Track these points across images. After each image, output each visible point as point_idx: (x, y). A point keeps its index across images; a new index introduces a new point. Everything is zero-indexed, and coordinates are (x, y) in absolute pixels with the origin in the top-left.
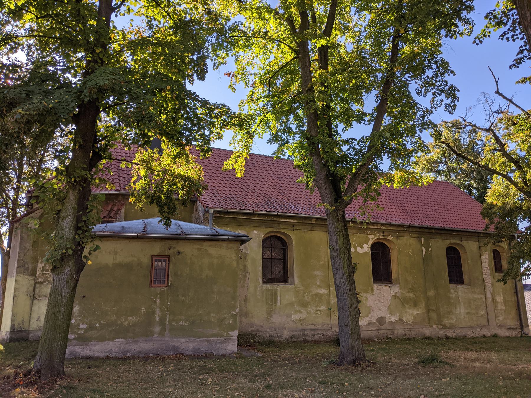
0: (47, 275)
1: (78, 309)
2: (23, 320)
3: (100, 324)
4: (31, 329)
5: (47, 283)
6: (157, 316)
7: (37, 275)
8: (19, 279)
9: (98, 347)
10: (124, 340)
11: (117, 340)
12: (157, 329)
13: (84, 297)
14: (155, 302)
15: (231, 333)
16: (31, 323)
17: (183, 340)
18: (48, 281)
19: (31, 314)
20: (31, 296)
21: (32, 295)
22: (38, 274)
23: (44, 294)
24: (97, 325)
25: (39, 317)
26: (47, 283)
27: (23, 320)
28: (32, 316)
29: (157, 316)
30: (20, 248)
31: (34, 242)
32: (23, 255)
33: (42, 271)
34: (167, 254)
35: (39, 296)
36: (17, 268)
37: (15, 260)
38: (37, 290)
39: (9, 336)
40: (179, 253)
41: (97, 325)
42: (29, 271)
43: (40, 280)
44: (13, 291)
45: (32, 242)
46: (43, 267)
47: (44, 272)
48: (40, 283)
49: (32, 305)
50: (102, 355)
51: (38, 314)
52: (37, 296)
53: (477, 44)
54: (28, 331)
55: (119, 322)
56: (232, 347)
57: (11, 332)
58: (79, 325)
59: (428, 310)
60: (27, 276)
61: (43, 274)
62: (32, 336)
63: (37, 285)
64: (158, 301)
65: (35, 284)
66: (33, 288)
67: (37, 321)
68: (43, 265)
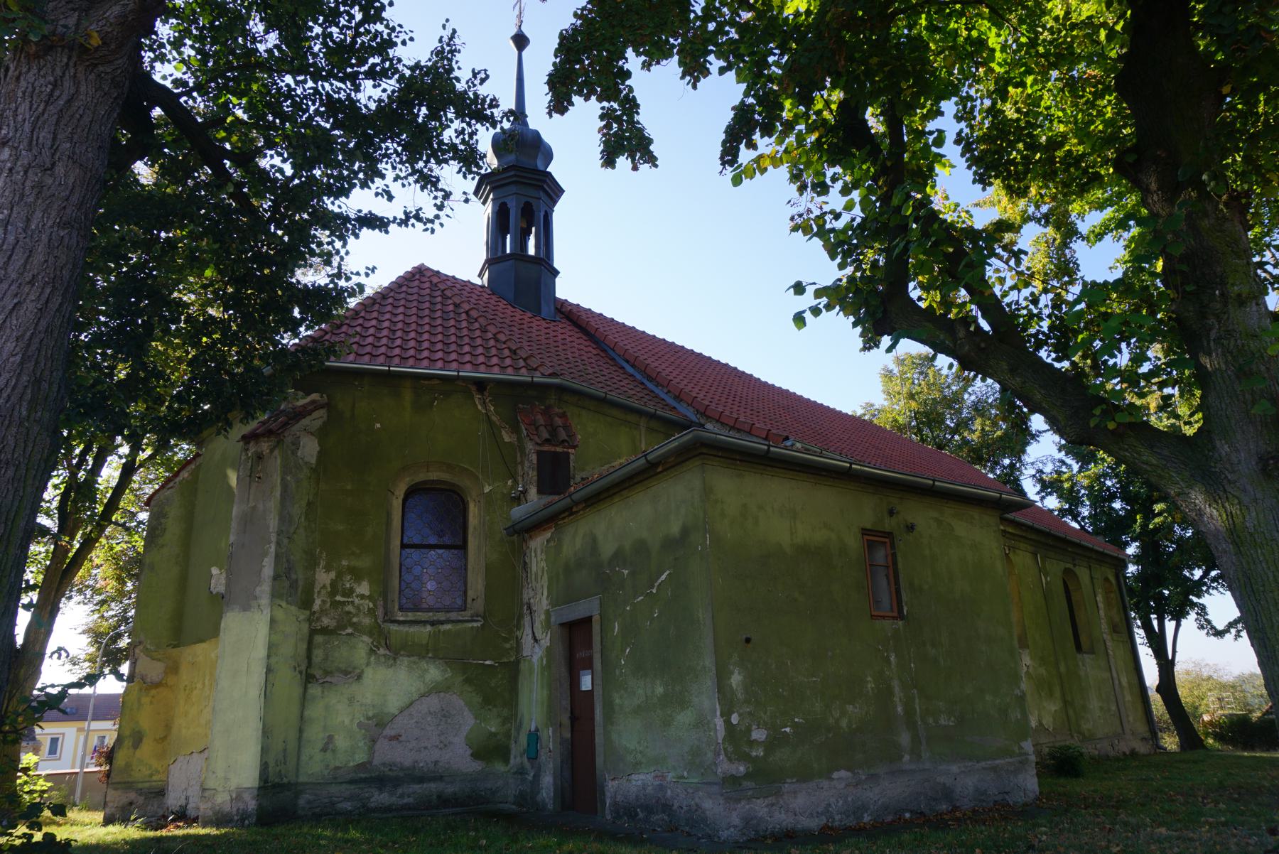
0: (349, 608)
1: (740, 678)
2: (285, 750)
3: (795, 726)
4: (302, 779)
5: (349, 630)
6: (898, 703)
7: (316, 607)
8: (280, 614)
9: (800, 801)
10: (849, 774)
11: (835, 775)
12: (905, 739)
13: (748, 640)
14: (888, 661)
15: (1024, 744)
16: (304, 758)
17: (955, 768)
18: (353, 625)
19: (301, 731)
20: (301, 673)
21: (303, 668)
22: (318, 602)
23: (343, 666)
24: (788, 730)
25: (330, 738)
26: (349, 630)
27: (285, 750)
28: (305, 735)
29: (896, 699)
30: (282, 519)
31: (309, 504)
32: (285, 541)
33: (333, 593)
34: (887, 528)
35: (327, 673)
36: (276, 577)
37: (265, 554)
38: (318, 654)
39: (252, 805)
40: (911, 528)
41: (788, 730)
42: (300, 589)
43: (326, 621)
44: (261, 652)
45: (304, 503)
46: (333, 584)
47: (338, 598)
48: (325, 631)
49: (304, 700)
50: (814, 824)
51: (325, 728)
52: (317, 673)
53: (347, 253)
54: (297, 784)
55: (831, 721)
56: (1030, 783)
57: (259, 788)
58: (749, 730)
59: (1065, 702)
60: (293, 608)
61: (335, 604)
62: (309, 802)
63: (319, 639)
64: (892, 658)
65: (313, 632)
66: (305, 646)
67: (324, 750)
68: (333, 575)
